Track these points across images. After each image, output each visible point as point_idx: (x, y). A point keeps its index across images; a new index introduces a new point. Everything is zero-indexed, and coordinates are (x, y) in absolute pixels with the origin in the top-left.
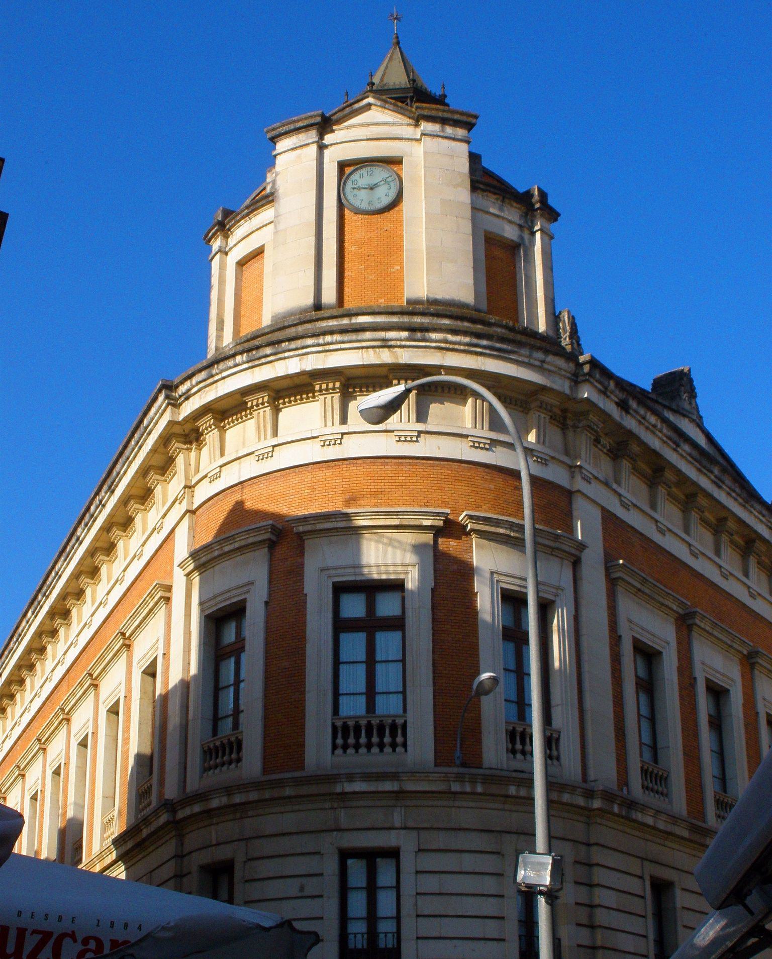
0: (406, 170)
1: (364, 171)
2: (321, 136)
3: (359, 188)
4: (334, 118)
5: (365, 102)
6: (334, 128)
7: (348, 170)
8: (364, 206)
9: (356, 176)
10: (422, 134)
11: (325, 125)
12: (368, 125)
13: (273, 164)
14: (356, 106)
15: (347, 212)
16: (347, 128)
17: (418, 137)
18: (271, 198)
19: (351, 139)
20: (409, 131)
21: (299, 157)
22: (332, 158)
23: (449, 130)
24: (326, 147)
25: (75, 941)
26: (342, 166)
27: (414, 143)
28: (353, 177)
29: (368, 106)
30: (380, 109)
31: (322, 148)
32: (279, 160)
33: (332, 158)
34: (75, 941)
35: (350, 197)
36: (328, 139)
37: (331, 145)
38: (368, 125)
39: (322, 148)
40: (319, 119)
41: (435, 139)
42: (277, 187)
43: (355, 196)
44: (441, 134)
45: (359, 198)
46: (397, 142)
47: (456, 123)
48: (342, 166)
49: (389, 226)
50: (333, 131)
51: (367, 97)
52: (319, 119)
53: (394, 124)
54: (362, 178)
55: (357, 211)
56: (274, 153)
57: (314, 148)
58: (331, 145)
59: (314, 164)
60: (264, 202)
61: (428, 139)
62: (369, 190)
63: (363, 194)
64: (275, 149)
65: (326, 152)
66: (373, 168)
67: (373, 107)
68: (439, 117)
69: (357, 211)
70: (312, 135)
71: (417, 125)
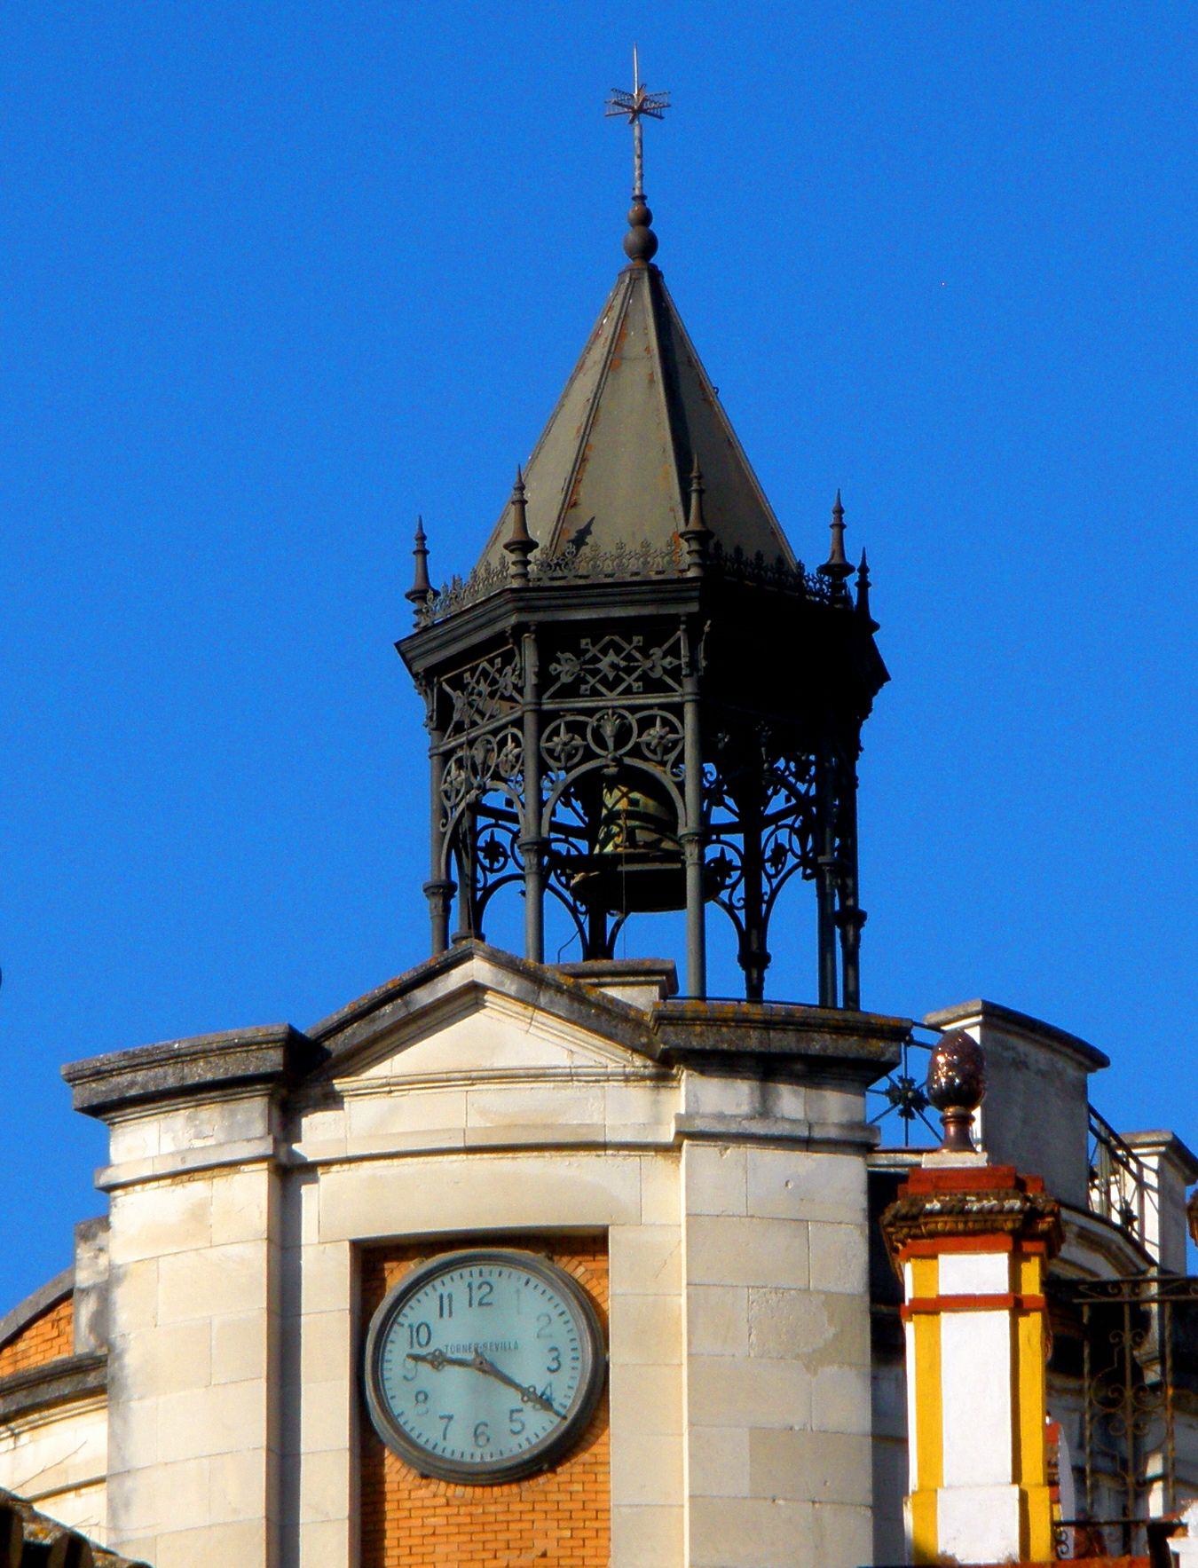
0: (619, 1285)
1: (455, 1285)
2: (286, 1123)
3: (439, 1361)
4: (335, 1045)
5: (455, 979)
6: (339, 1084)
7: (398, 1276)
8: (458, 1445)
9: (423, 1308)
10: (682, 1135)
11: (301, 1075)
12: (473, 1079)
13: (95, 1222)
14: (424, 996)
15: (394, 1471)
16: (390, 1087)
17: (668, 1135)
18: (92, 1380)
19: (394, 1149)
20: (634, 1108)
21: (199, 1214)
22: (334, 1215)
23: (791, 1102)
24: (309, 1170)
25: (520, 1411)
26: (371, 1259)
27: (658, 1163)
28: (414, 1313)
29: (472, 996)
30: (518, 1007)
31: (289, 1174)
32: (128, 1211)
33: (334, 1215)
34: (520, 1411)
35: (402, 1405)
36: (319, 1133)
37: (328, 1164)
38: (473, 1079)
39: (289, 1174)
40: (273, 1060)
41: (733, 1152)
42: (114, 1336)
43: (422, 1396)
44: (757, 1128)
45: (445, 1411)
46: (583, 1158)
47: (815, 1072)
48: (371, 1259)
49: (550, 1537)
50: (332, 1100)
51: (466, 957)
52: (273, 1060)
53: (571, 1076)
54: (447, 1314)
55: (432, 1468)
56: (106, 1178)
57: (255, 1185)
58: (328, 1164)
59: (256, 1257)
60: (64, 1387)
61: (708, 1151)
62: (484, 1362)
63: (453, 1388)
64: (106, 1163)
65: (312, 1197)
66: (491, 1272)
67: (488, 997)
68: (752, 1055)
69: (432, 1468)
70: (253, 1112)
71: (662, 1075)
